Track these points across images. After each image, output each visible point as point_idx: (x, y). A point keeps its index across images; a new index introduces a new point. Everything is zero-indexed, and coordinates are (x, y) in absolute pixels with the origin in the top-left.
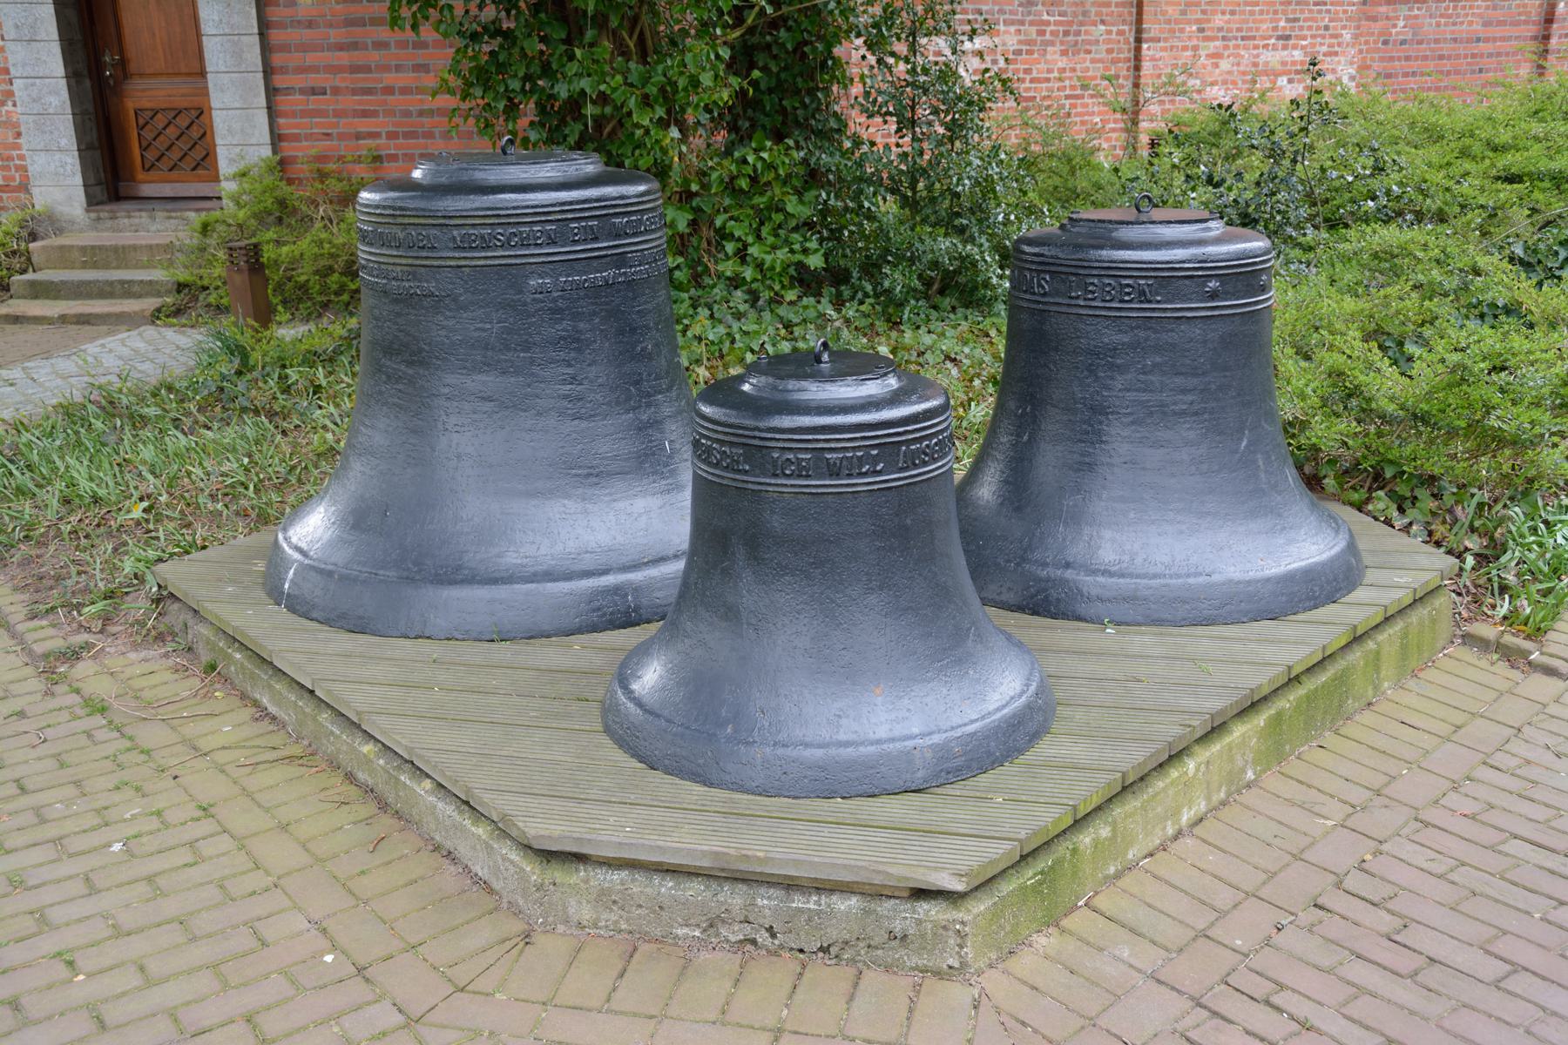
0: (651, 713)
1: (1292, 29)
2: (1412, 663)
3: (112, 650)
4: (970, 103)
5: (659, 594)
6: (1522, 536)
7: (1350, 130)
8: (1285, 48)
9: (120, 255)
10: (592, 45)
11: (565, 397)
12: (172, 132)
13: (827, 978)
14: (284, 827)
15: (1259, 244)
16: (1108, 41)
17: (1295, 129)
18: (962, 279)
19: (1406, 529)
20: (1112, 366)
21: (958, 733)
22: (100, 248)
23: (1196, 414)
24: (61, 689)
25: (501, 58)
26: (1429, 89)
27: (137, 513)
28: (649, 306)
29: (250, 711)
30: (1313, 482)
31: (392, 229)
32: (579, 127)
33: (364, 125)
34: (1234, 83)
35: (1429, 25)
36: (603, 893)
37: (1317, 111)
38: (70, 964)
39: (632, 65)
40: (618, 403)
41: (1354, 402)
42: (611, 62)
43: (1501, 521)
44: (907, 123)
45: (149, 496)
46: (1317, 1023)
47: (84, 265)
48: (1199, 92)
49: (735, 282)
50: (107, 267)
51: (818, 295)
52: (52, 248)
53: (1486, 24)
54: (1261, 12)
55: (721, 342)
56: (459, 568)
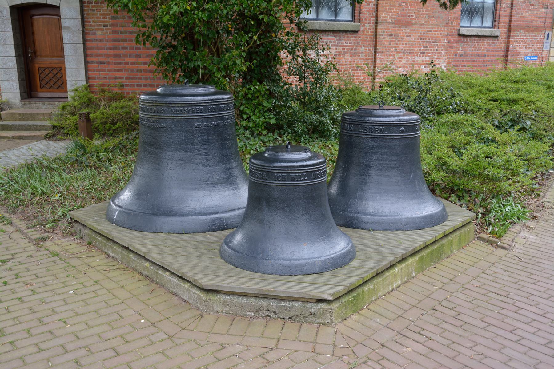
0: (236, 251)
1: (425, 50)
2: (462, 245)
3: (56, 238)
4: (323, 72)
5: (233, 220)
6: (496, 208)
7: (444, 84)
8: (423, 56)
9: (33, 116)
10: (202, 51)
11: (205, 159)
12: (51, 75)
13: (292, 327)
14: (122, 287)
15: (416, 117)
16: (365, 52)
17: (427, 83)
18: (320, 129)
19: (461, 205)
20: (372, 153)
21: (329, 257)
22: (26, 114)
23: (397, 167)
24: (42, 249)
25: (172, 54)
26: (470, 71)
27: (57, 197)
28: (230, 132)
29: (104, 256)
30: (433, 191)
31: (149, 107)
32: (196, 77)
33: (118, 74)
34: (407, 67)
35: (469, 50)
36: (225, 302)
37: (433, 77)
38: (65, 322)
39: (215, 58)
40: (220, 162)
41: (445, 167)
42: (208, 56)
43: (490, 203)
44: (302, 78)
45: (61, 192)
46: (433, 338)
47: (20, 120)
48: (395, 70)
49: (246, 128)
50: (28, 120)
51: (273, 133)
52: (9, 113)
53: (487, 51)
54: (415, 44)
55: (243, 147)
56: (172, 211)
